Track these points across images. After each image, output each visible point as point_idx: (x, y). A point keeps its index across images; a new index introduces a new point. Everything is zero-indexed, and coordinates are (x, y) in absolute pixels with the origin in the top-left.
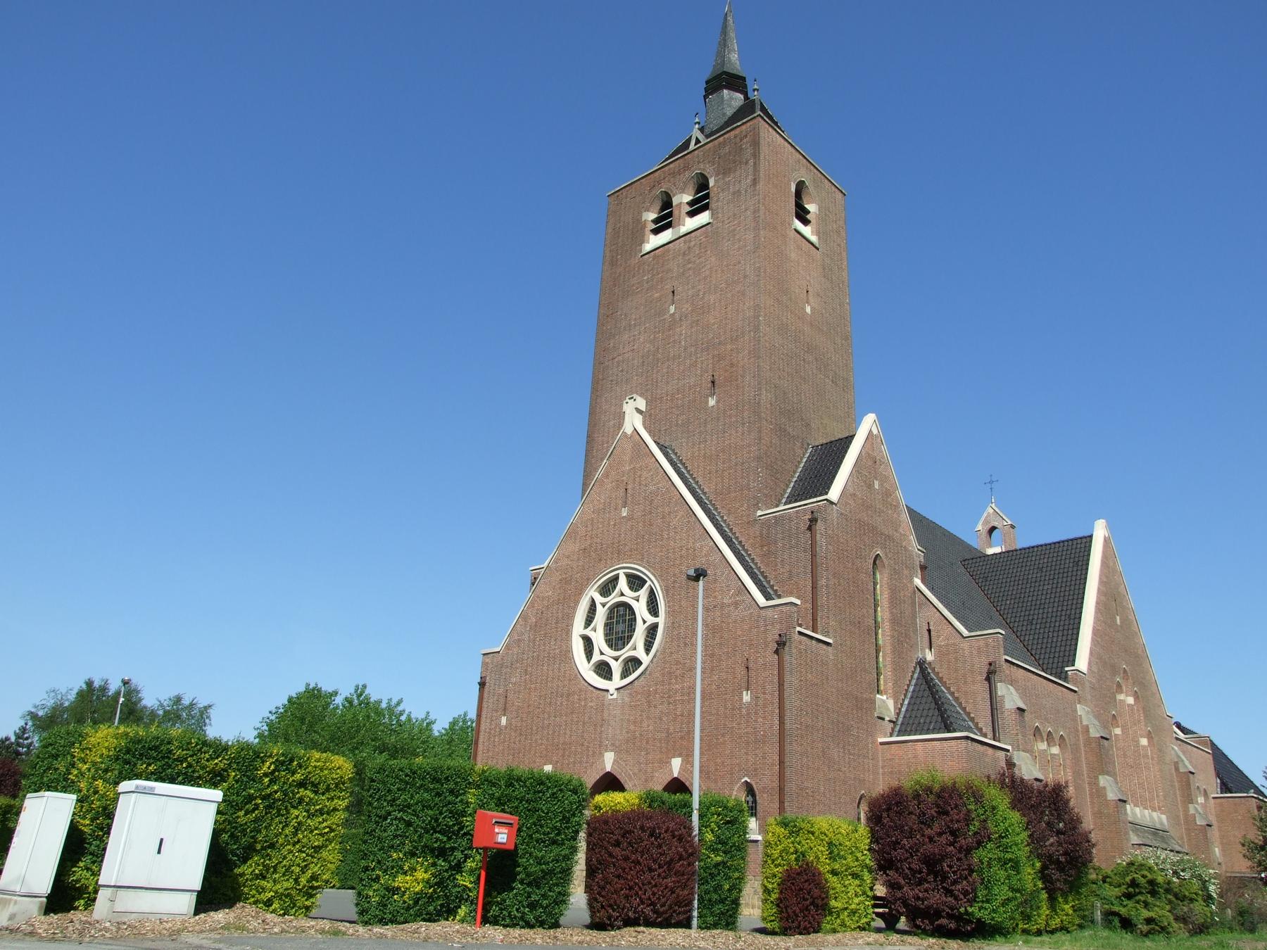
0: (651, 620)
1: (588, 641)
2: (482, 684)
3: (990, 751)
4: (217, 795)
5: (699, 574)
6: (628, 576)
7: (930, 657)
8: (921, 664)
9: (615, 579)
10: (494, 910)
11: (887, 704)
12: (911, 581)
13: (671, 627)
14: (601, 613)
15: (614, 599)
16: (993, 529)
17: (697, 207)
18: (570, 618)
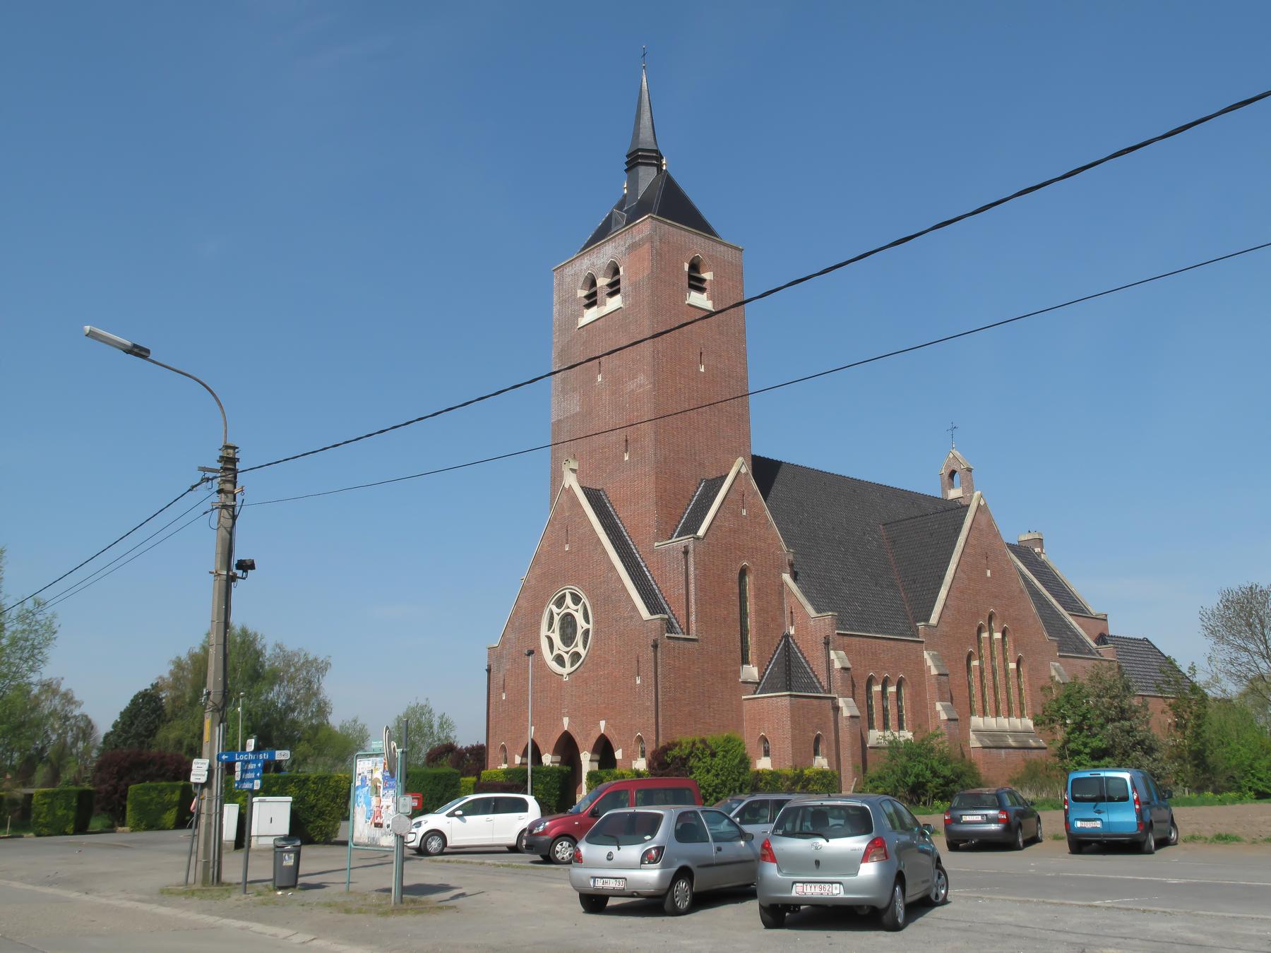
0: (586, 626)
1: (550, 639)
2: (489, 671)
3: (815, 702)
4: (290, 799)
5: (531, 653)
6: (572, 594)
7: (792, 632)
8: (787, 636)
9: (564, 596)
10: (788, 826)
11: (751, 672)
12: (780, 575)
13: (596, 632)
14: (557, 619)
15: (564, 611)
16: (953, 473)
17: (614, 289)
18: (538, 624)
